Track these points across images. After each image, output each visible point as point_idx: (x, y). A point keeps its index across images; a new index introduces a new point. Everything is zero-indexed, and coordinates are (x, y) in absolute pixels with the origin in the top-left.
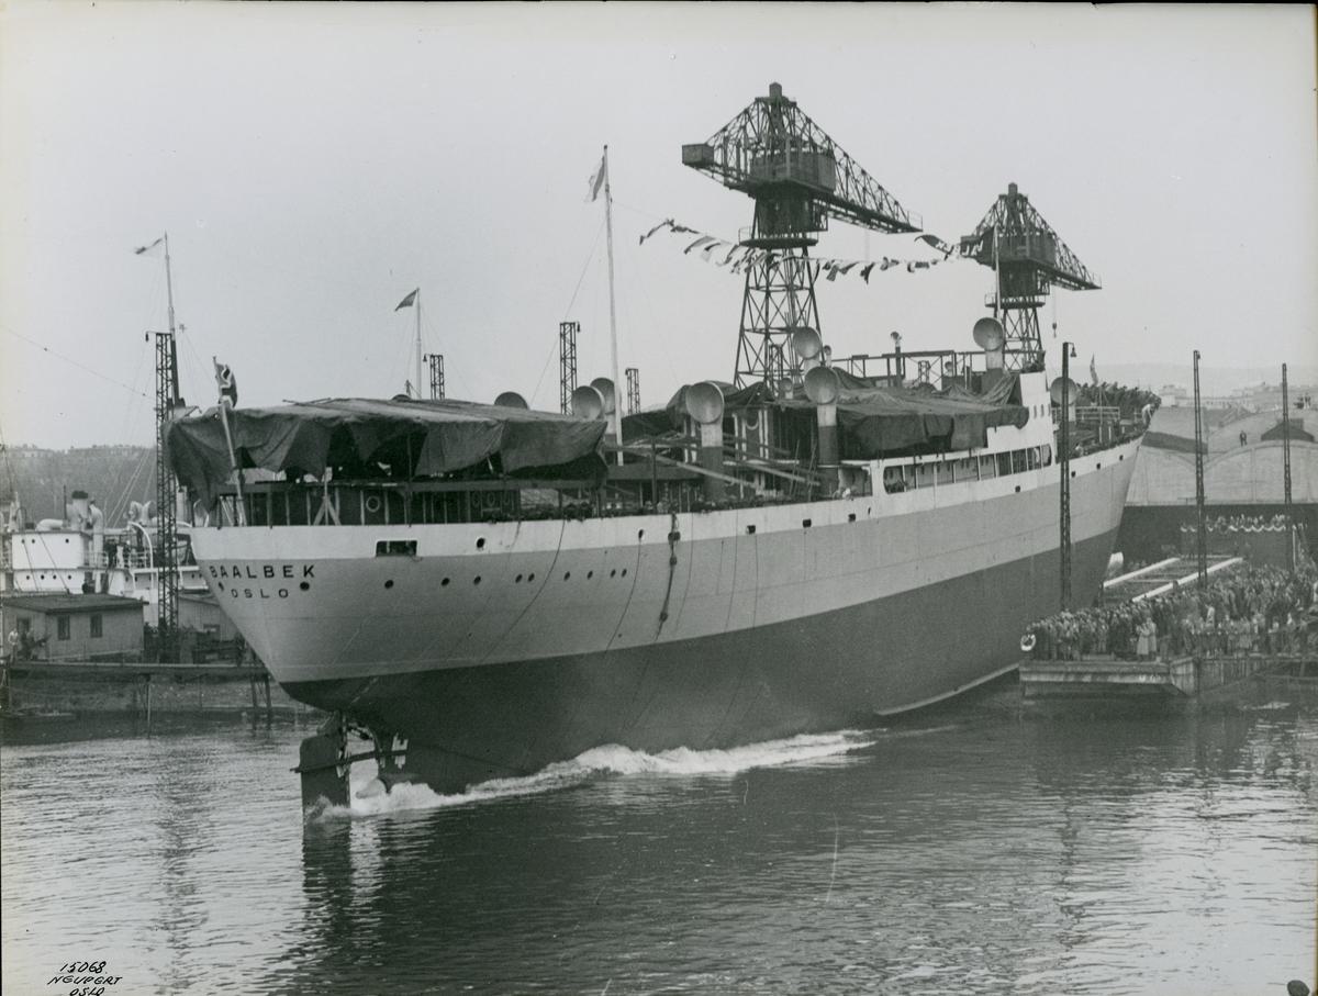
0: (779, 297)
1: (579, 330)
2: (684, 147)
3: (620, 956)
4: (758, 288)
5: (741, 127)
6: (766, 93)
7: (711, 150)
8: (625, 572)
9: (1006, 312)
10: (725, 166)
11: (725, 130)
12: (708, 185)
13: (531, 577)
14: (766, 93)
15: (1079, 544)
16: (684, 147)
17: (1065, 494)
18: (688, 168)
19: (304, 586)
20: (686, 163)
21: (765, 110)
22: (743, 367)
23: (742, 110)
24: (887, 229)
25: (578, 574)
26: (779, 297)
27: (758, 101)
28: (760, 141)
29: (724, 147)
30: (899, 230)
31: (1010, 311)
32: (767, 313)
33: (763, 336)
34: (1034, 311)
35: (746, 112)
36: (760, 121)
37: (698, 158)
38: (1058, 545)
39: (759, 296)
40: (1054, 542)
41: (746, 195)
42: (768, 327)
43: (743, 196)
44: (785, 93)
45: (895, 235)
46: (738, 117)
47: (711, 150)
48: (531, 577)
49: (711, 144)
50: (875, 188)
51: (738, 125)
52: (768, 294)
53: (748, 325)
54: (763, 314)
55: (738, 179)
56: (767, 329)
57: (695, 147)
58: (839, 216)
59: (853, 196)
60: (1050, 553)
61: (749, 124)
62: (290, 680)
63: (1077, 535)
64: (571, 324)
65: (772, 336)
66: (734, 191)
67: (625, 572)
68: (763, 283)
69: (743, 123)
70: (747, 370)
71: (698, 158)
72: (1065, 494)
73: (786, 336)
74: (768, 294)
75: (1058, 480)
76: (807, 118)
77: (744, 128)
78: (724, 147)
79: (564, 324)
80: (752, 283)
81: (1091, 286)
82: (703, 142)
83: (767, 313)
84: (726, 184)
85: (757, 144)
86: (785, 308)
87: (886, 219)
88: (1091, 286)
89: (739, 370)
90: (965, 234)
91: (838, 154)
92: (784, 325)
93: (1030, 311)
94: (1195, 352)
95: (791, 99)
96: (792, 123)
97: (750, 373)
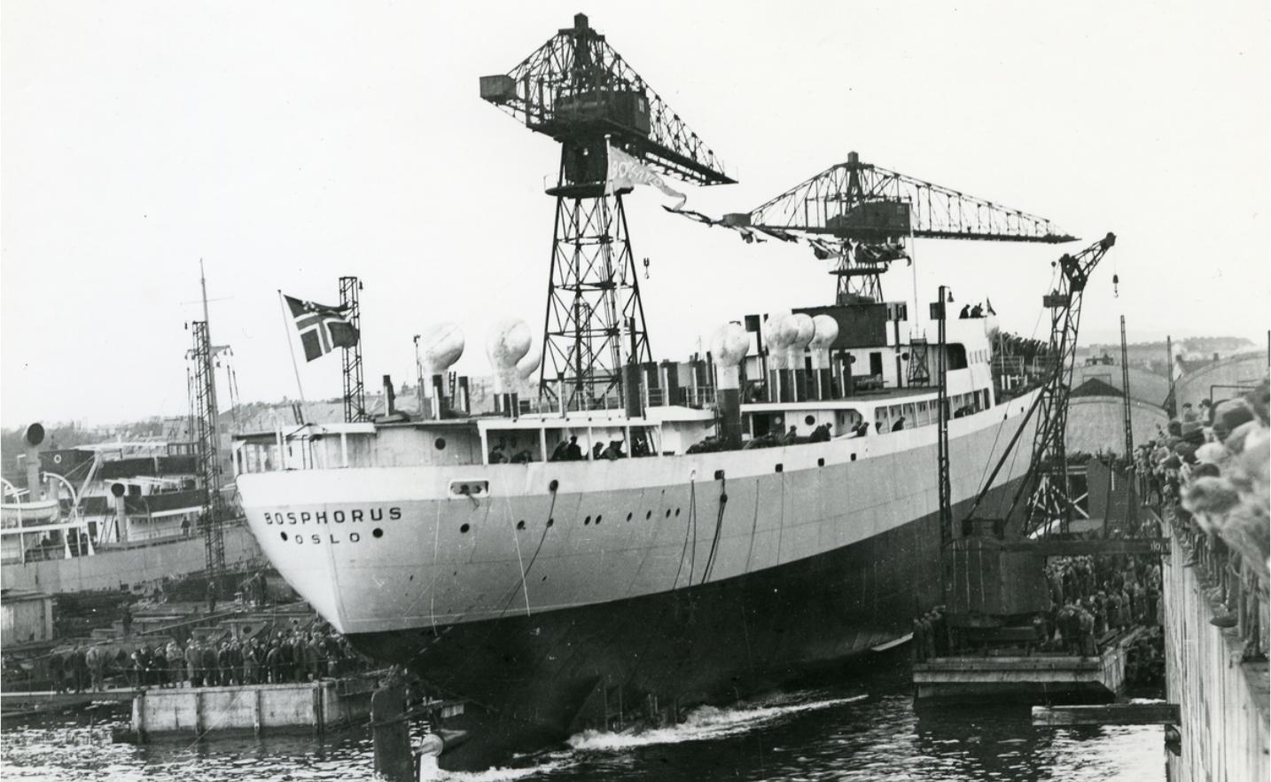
0: (590, 250)
1: (361, 288)
2: (483, 79)
3: (1056, 504)
4: (567, 240)
5: (545, 60)
6: (571, 25)
7: (513, 83)
8: (678, 511)
9: (578, 203)
10: (528, 102)
11: (526, 62)
12: (508, 122)
13: (599, 519)
14: (571, 25)
15: (957, 505)
16: (483, 79)
17: (944, 461)
18: (486, 103)
19: (378, 533)
20: (483, 97)
21: (570, 42)
22: (553, 327)
23: (545, 42)
24: (700, 180)
25: (613, 515)
26: (590, 250)
27: (562, 33)
28: (565, 77)
29: (526, 78)
30: (713, 182)
31: (584, 201)
32: (578, 269)
33: (574, 293)
34: (877, 277)
35: (550, 44)
36: (565, 52)
37: (498, 90)
38: (937, 508)
39: (568, 249)
40: (934, 506)
41: (551, 139)
42: (580, 283)
43: (548, 140)
44: (591, 25)
45: (708, 187)
46: (541, 49)
47: (513, 83)
48: (599, 519)
49: (513, 76)
50: (689, 135)
51: (541, 57)
52: (579, 247)
53: (557, 281)
54: (574, 268)
55: (541, 117)
56: (578, 286)
57: (495, 78)
58: (687, 178)
59: (668, 142)
60: (934, 514)
61: (553, 57)
62: (352, 632)
63: (955, 499)
64: (352, 278)
65: (583, 294)
66: (538, 134)
67: (678, 511)
68: (573, 234)
69: (547, 56)
70: (558, 331)
71: (498, 90)
72: (944, 461)
73: (601, 292)
74: (579, 247)
75: (936, 440)
76: (616, 54)
77: (548, 60)
78: (526, 78)
79: (344, 279)
80: (561, 235)
81: (728, 181)
82: (505, 74)
83: (578, 269)
84: (529, 125)
85: (562, 81)
86: (600, 262)
87: (702, 169)
88: (728, 181)
89: (549, 331)
90: (1046, 294)
91: (649, 94)
92: (598, 281)
93: (873, 276)
94: (1122, 317)
95: (599, 32)
96: (600, 58)
97: (561, 333)
